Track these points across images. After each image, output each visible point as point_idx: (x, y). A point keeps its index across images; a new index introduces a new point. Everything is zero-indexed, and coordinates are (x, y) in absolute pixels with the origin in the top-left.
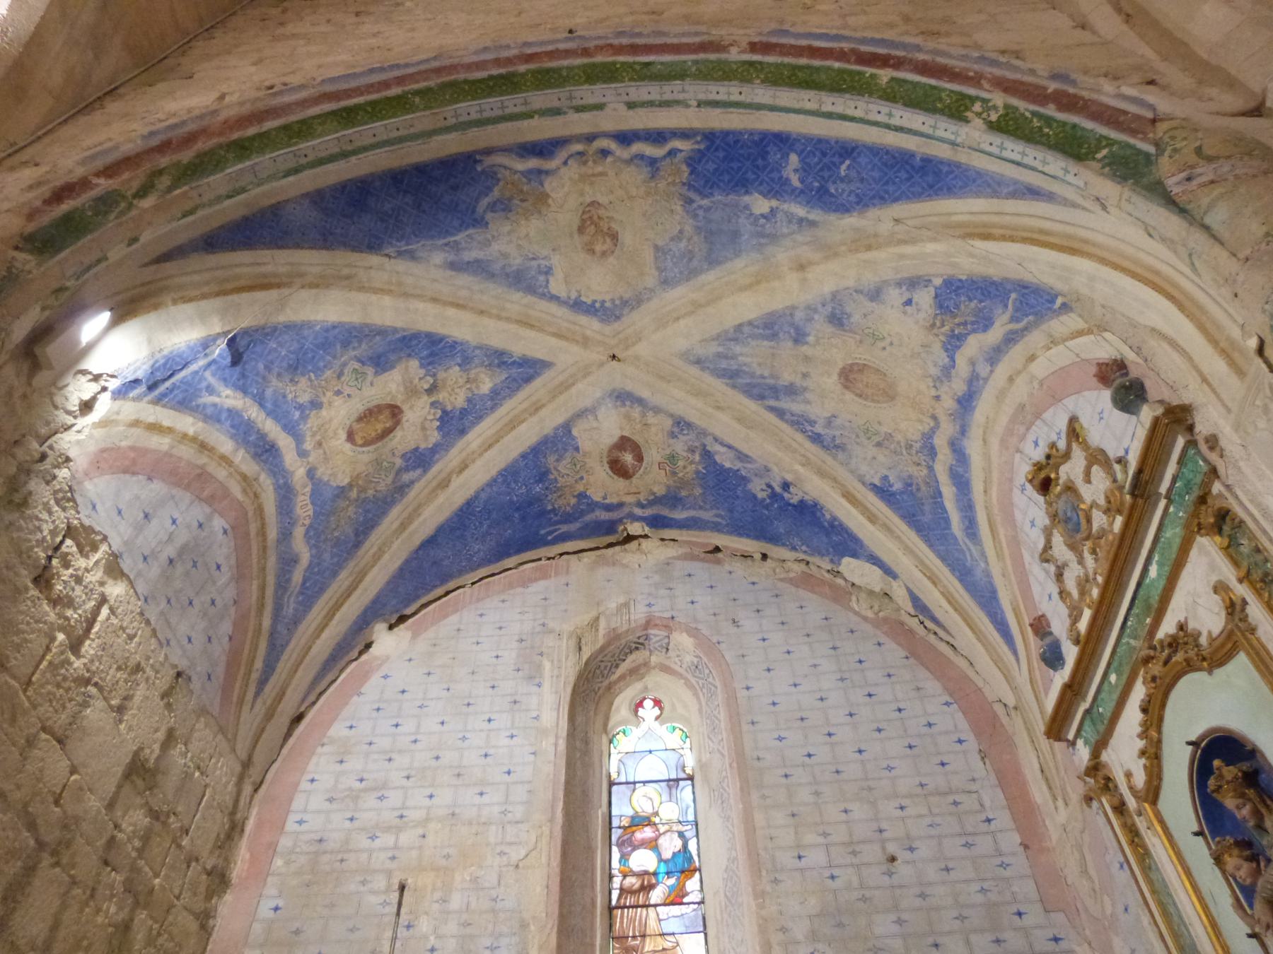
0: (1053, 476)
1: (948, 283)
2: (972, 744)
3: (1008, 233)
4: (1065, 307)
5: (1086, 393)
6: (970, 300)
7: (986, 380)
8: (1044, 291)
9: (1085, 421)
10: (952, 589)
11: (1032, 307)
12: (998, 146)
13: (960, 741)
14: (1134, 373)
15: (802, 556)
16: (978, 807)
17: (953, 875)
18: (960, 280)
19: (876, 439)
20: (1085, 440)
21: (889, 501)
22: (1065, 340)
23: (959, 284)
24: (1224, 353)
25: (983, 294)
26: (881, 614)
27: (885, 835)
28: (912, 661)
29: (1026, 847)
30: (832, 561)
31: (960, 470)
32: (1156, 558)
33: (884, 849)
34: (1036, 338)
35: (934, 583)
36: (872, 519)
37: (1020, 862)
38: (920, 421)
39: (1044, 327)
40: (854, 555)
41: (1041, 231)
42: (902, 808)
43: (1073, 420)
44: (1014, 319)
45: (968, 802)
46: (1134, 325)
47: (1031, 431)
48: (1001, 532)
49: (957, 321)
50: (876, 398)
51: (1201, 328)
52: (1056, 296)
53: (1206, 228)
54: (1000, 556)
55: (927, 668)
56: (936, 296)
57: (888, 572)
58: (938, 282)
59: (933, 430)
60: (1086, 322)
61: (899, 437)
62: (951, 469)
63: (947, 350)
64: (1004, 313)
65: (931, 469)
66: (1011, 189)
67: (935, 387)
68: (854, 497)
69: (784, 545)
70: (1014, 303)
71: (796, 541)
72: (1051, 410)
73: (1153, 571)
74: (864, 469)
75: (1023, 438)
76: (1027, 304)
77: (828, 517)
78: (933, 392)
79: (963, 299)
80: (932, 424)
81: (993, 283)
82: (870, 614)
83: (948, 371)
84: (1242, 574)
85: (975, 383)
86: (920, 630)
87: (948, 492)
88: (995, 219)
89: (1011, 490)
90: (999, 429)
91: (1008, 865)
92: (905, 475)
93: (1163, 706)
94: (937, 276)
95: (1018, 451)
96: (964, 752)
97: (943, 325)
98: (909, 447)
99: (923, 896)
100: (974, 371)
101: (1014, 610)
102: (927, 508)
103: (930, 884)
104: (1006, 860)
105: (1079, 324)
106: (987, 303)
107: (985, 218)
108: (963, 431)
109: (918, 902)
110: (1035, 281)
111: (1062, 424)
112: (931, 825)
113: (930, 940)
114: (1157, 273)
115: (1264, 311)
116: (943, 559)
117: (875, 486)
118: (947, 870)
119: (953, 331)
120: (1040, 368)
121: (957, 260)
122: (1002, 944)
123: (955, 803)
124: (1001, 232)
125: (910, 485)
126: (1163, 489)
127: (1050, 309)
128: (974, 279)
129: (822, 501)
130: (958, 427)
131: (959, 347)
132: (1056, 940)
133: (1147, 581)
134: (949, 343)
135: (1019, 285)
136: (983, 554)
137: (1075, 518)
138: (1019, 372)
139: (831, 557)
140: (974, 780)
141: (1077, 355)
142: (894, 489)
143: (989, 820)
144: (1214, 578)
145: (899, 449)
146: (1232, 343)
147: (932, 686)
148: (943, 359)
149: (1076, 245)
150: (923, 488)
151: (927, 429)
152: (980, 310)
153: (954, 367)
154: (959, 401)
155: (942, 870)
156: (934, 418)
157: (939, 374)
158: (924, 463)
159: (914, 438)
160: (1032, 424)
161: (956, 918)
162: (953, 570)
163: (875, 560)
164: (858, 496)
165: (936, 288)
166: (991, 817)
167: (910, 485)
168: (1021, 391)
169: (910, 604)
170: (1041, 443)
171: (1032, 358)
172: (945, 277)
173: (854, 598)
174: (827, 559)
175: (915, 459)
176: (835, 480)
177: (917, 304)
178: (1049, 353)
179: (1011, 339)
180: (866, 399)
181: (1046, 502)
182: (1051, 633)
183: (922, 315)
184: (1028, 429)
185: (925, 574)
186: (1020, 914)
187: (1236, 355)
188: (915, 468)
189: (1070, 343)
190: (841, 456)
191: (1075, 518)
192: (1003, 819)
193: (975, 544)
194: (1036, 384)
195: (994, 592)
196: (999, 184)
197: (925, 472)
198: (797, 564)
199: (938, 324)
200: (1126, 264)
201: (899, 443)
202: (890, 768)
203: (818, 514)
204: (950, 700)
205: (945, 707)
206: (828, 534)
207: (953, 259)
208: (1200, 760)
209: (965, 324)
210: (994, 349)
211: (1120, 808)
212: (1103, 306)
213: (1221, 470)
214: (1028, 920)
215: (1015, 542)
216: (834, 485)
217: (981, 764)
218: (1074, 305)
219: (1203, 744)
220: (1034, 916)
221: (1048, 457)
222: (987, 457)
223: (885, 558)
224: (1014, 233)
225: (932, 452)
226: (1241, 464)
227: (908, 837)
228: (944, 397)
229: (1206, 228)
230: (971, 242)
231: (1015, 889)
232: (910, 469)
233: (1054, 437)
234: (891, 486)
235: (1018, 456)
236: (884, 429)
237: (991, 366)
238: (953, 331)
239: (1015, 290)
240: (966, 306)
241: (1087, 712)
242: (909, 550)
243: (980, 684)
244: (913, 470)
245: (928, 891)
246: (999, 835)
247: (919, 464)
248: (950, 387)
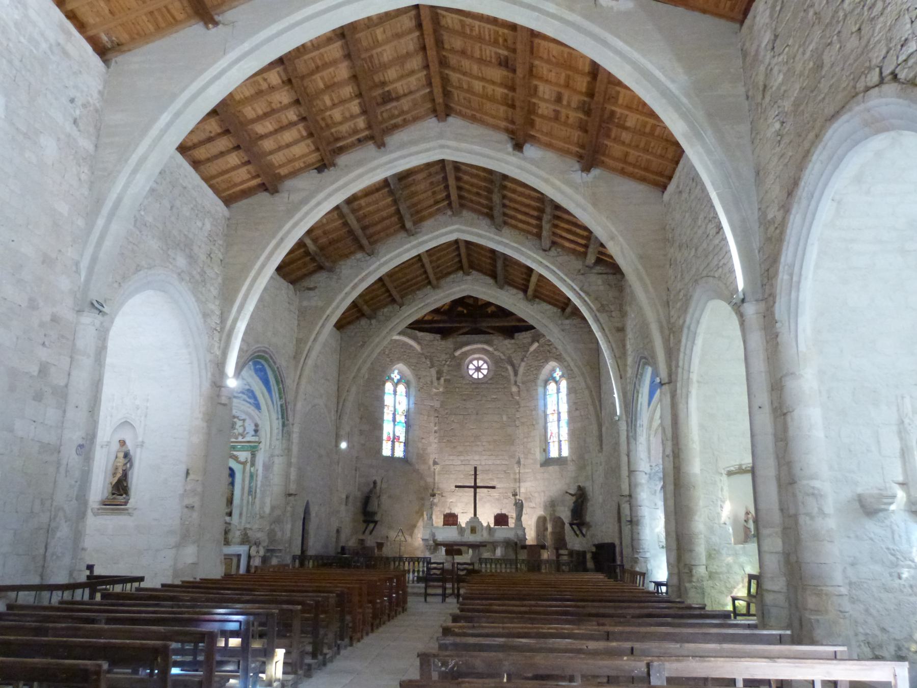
179: (250, 403)
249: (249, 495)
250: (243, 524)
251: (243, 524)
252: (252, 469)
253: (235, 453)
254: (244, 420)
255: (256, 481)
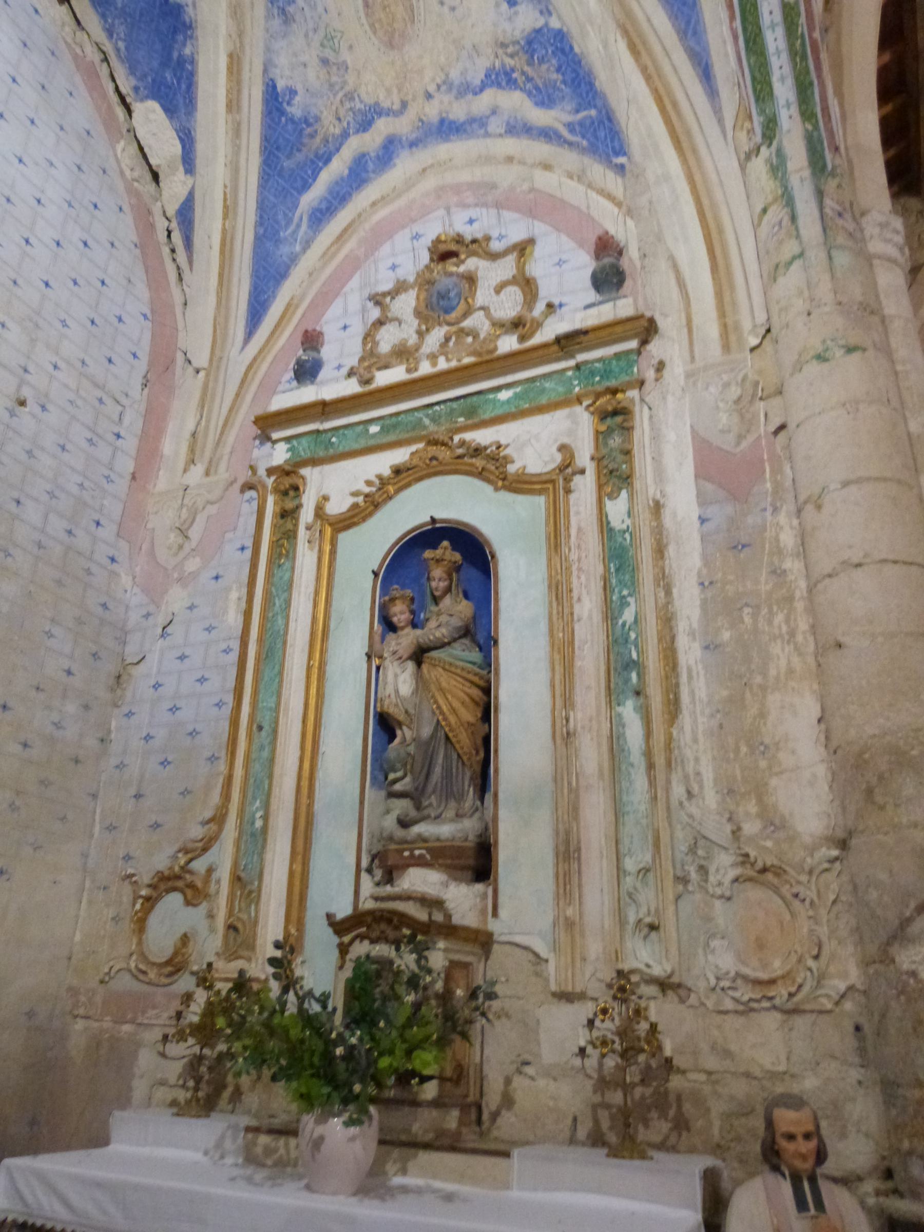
0: (463, 257)
1: (560, 36)
2: (142, 365)
3: (651, 69)
4: (621, 169)
5: (564, 238)
6: (558, 70)
7: (487, 135)
8: (619, 139)
9: (539, 251)
10: (239, 236)
11: (596, 138)
12: (772, 21)
13: (135, 355)
14: (625, 263)
15: (108, 47)
16: (117, 419)
17: (66, 456)
18: (571, 48)
19: (328, 53)
20: (524, 264)
21: (270, 113)
22: (590, 186)
23: (567, 49)
24: (724, 327)
25: (573, 81)
26: (136, 184)
27: (28, 377)
28: (138, 251)
29: (134, 477)
30: (136, 89)
31: (371, 166)
32: (518, 389)
33: (19, 387)
34: (570, 159)
35: (225, 216)
36: (233, 105)
37: (121, 486)
38: (389, 91)
39: (587, 160)
40: (170, 111)
41: (675, 104)
42: (55, 367)
43: (531, 242)
44: (570, 127)
45: (112, 409)
46: (659, 238)
47: (478, 209)
48: (351, 245)
49: (526, 68)
50: (377, 26)
51: (719, 295)
52: (625, 154)
53: (830, 258)
54: (327, 256)
55: (147, 272)
56: (538, 31)
57: (188, 161)
58: (555, 23)
59: (389, 112)
60: (624, 196)
61: (351, 79)
62: (363, 155)
63: (487, 76)
64: (570, 112)
65: (345, 135)
66: (698, 48)
67: (439, 87)
68: (239, 72)
69: (103, 16)
70: (585, 118)
71: (121, 30)
72: (516, 215)
73: (504, 395)
74: (282, 60)
75: (465, 206)
76: (595, 130)
77: (187, 51)
78: (432, 88)
79: (554, 62)
80: (396, 107)
81: (591, 85)
82: (128, 173)
83: (466, 90)
84: (597, 456)
85: (475, 126)
86: (162, 236)
87: (338, 167)
88: (657, 49)
89: (403, 227)
90: (450, 178)
91: (112, 481)
92: (314, 111)
93: (421, 479)
94: (560, 18)
95: (448, 210)
96: (132, 367)
97: (512, 56)
98: (350, 97)
99: (30, 453)
100: (488, 117)
101: (289, 305)
102: (299, 157)
103: (43, 449)
104: (113, 476)
105: (619, 193)
106: (567, 90)
107: (652, 39)
108: (413, 144)
109: (23, 457)
110: (623, 125)
111: (517, 234)
112: (71, 402)
113: (16, 495)
114: (721, 231)
115: (824, 341)
116: (262, 207)
117: (274, 87)
118: (63, 448)
119: (513, 70)
120: (545, 181)
121: (592, 34)
122: (72, 538)
123: (101, 401)
124: (649, 63)
125: (309, 125)
126: (581, 357)
127: (608, 156)
128: (583, 63)
129: (199, 33)
130: (414, 135)
131: (499, 86)
132: (113, 560)
133: (491, 396)
134: (497, 75)
135: (607, 113)
136: (307, 245)
137: (455, 303)
138: (522, 162)
139: (140, 84)
140: (127, 395)
141: (588, 207)
142: (289, 109)
143: (118, 436)
144: (566, 440)
145: (337, 88)
146: (737, 327)
147: (142, 290)
148: (477, 78)
149: (685, 145)
150: (318, 140)
151: (386, 104)
152: (554, 87)
153: (475, 94)
154: (442, 121)
155: (59, 445)
156: (404, 105)
157: (456, 82)
158: (345, 124)
159: (364, 96)
160: (485, 205)
161: (48, 493)
162: (260, 222)
163: (187, 140)
164: (246, 75)
165: (546, 24)
166: (122, 434)
167: (309, 125)
168: (506, 177)
169: (177, 206)
170: (476, 225)
171: (547, 167)
172: (565, 29)
173: (122, 143)
174: (133, 82)
175: (342, 113)
176: (241, 34)
177: (516, 13)
178: (569, 181)
179: (547, 134)
180: (367, 15)
181: (427, 267)
182: (319, 352)
183: (507, 26)
184: (476, 205)
185: (225, 200)
186: (98, 524)
187: (733, 338)
188: (331, 118)
189: (593, 195)
190: (277, 22)
191: (455, 303)
192: (130, 444)
193: (310, 227)
194: (525, 187)
195: (282, 275)
196: (695, 33)
197: (337, 131)
198: (95, 49)
199: (510, 50)
200: (705, 202)
201: (345, 83)
202: (64, 323)
203: (180, 37)
204: (149, 315)
205: (142, 318)
206: (166, 62)
207: (589, 28)
208: (420, 534)
209: (529, 79)
210: (525, 125)
211: (288, 515)
212: (651, 202)
213: (648, 386)
214: (101, 532)
215: (353, 265)
216: (234, 36)
217: (139, 387)
218: (628, 175)
219: (438, 525)
220: (108, 532)
221: (474, 241)
222: (409, 184)
223: (201, 147)
224: (656, 78)
225: (365, 125)
226: (670, 398)
227: (47, 396)
228: (435, 102)
229: (830, 258)
230: (619, 38)
231: (105, 502)
232: (325, 113)
233: (495, 234)
234: (289, 103)
235: (442, 212)
236: (346, 56)
237: (506, 132)
238: (513, 70)
239: (600, 112)
240: (548, 70)
241: (318, 432)
242: (235, 169)
243: (180, 325)
244: (328, 118)
245: (36, 452)
246: (119, 453)
247: (339, 119)
248: (450, 103)
249: (612, 695)
250: (594, 948)
251: (594, 948)
252: (617, 509)
253: (482, 437)
254: (523, 249)
255: (664, 582)
